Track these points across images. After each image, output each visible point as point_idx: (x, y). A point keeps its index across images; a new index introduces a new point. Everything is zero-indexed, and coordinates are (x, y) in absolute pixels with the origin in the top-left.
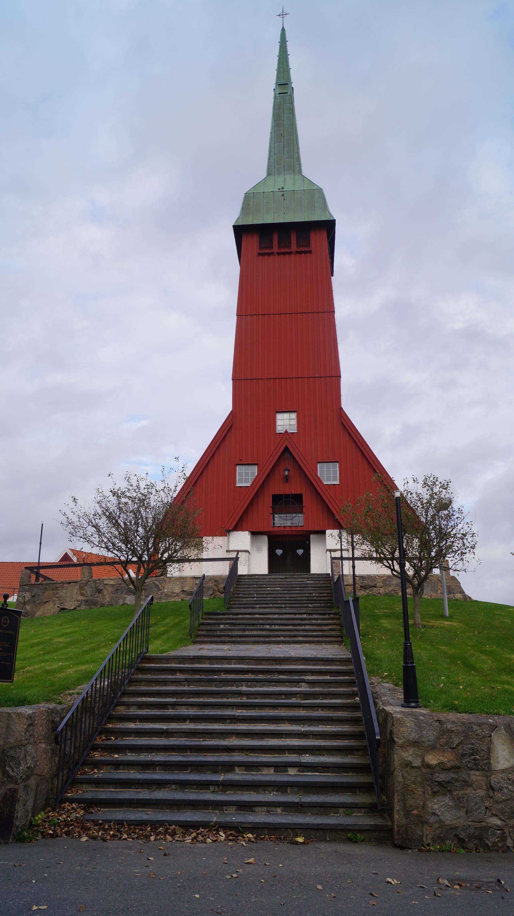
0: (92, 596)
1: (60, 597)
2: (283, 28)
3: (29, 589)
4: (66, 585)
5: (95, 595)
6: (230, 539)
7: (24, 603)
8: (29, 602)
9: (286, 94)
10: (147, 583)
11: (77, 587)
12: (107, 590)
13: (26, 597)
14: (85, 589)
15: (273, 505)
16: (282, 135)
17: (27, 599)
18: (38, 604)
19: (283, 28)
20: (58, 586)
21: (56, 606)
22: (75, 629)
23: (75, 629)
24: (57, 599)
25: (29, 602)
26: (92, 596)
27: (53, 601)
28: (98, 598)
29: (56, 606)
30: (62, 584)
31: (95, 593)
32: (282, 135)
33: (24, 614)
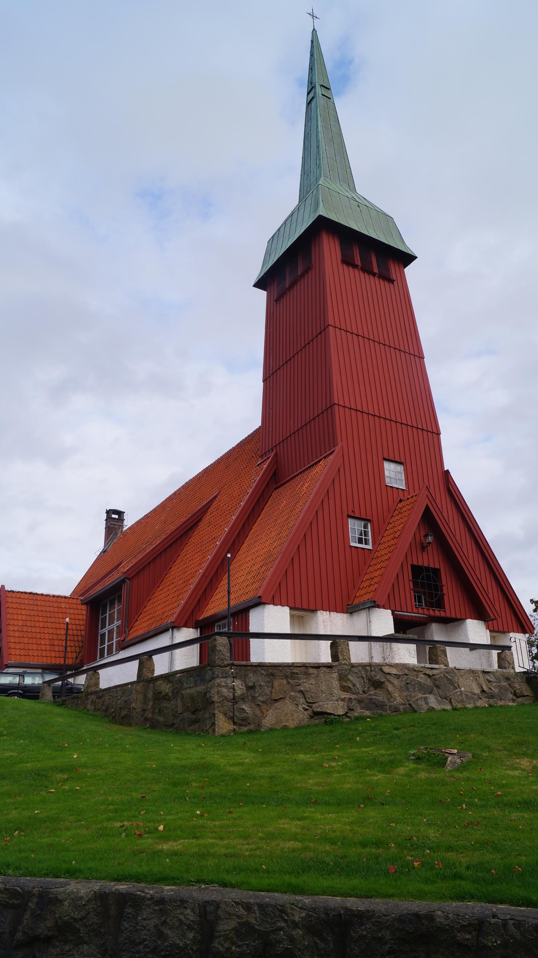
0: (364, 692)
1: (307, 691)
2: (314, 29)
3: (236, 673)
4: (311, 671)
5: (368, 691)
6: (371, 617)
7: (234, 699)
8: (243, 699)
9: (329, 99)
10: (437, 676)
11: (335, 675)
12: (392, 683)
13: (236, 688)
14: (349, 680)
15: (413, 578)
16: (331, 141)
17: (239, 693)
18: (263, 702)
19: (314, 29)
20: (295, 671)
21: (300, 708)
22: (12, 754)
23: (12, 754)
24: (299, 695)
25: (243, 699)
26: (364, 692)
27: (293, 699)
28: (380, 696)
29: (300, 708)
30: (303, 668)
31: (369, 688)
32: (331, 141)
33: (240, 722)
